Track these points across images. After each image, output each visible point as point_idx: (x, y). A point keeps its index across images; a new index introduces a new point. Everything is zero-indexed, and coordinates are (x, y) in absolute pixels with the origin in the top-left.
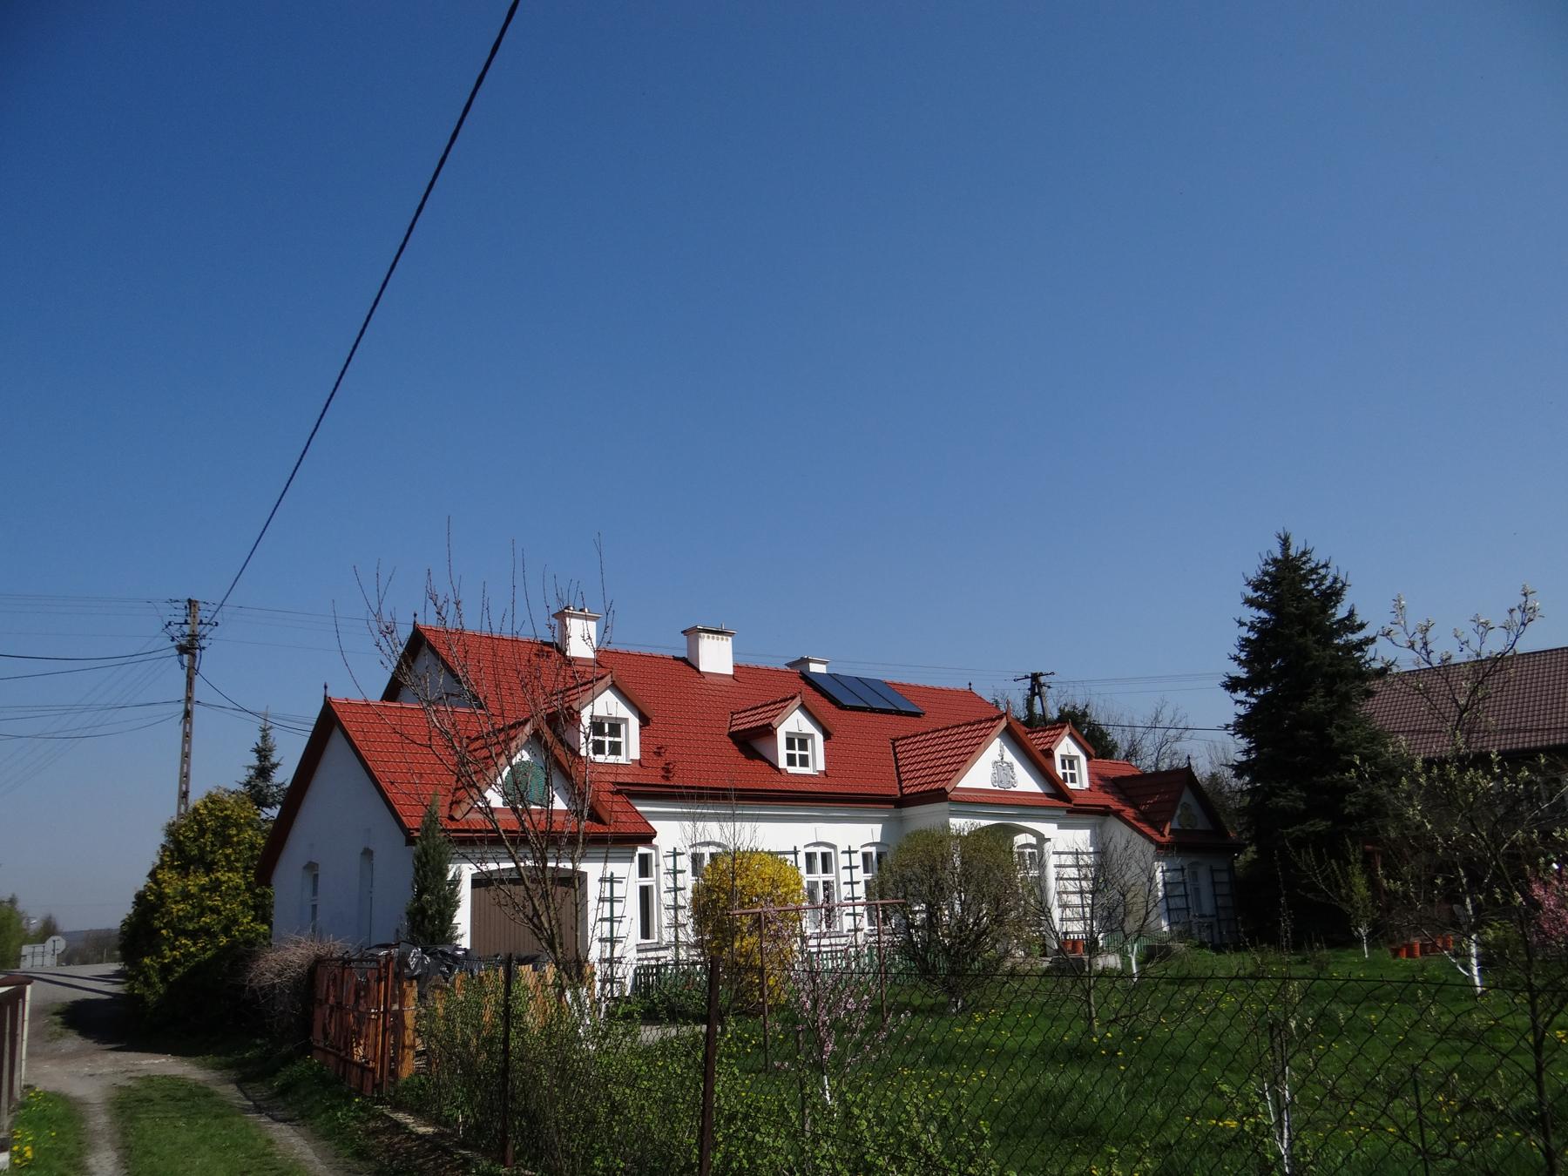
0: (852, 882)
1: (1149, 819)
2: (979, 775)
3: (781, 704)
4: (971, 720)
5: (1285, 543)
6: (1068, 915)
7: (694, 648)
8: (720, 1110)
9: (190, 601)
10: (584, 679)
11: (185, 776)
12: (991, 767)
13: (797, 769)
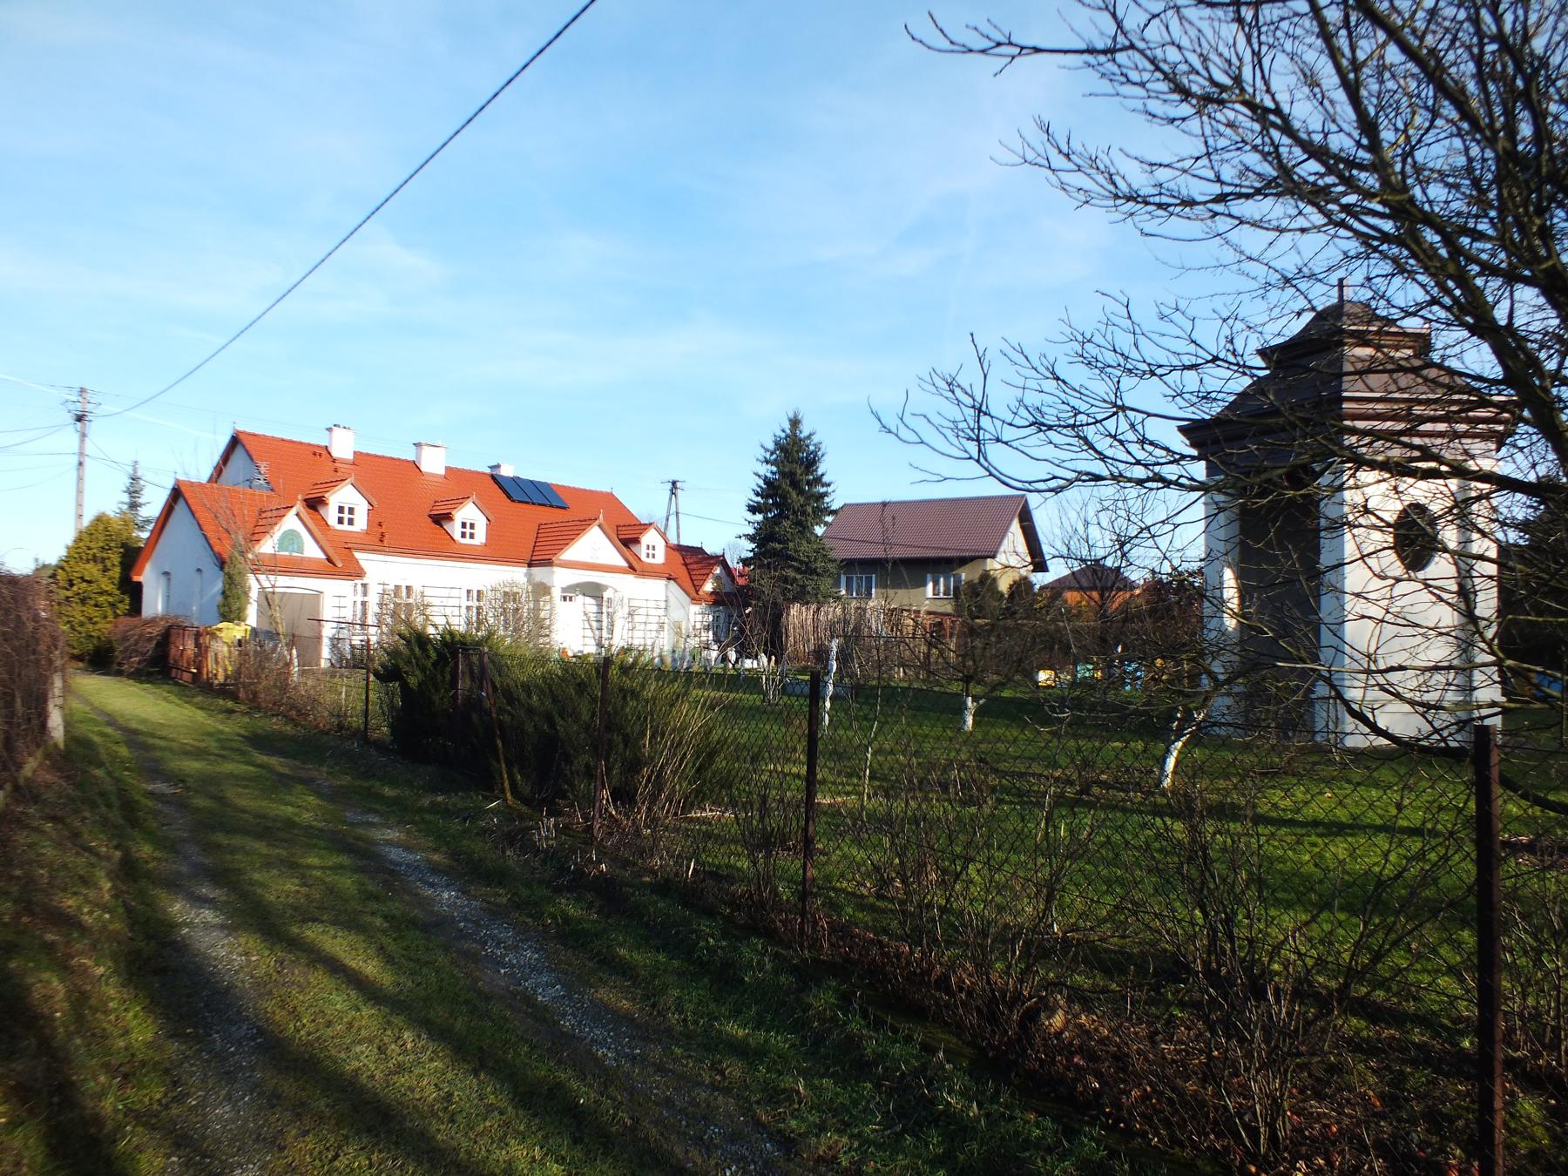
2: (578, 550)
5: (795, 423)
7: (419, 455)
8: (1513, 896)
9: (83, 391)
11: (79, 505)
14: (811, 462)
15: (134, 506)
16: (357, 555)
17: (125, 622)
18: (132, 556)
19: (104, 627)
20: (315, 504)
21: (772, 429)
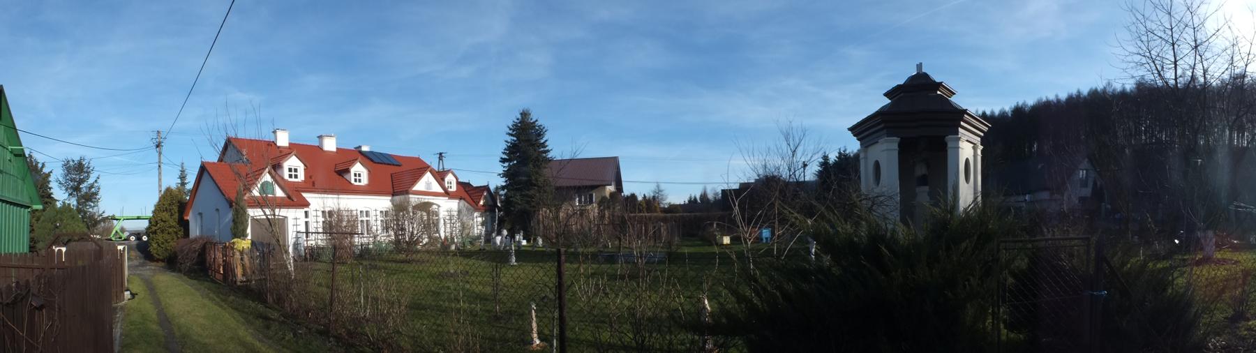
0: (377, 224)
1: (474, 203)
2: (420, 186)
3: (352, 162)
4: (419, 169)
7: (321, 143)
12: (427, 182)
13: (293, 180)
15: (183, 184)
16: (305, 195)
17: (182, 241)
18: (183, 207)
19: (173, 244)
20: (277, 167)
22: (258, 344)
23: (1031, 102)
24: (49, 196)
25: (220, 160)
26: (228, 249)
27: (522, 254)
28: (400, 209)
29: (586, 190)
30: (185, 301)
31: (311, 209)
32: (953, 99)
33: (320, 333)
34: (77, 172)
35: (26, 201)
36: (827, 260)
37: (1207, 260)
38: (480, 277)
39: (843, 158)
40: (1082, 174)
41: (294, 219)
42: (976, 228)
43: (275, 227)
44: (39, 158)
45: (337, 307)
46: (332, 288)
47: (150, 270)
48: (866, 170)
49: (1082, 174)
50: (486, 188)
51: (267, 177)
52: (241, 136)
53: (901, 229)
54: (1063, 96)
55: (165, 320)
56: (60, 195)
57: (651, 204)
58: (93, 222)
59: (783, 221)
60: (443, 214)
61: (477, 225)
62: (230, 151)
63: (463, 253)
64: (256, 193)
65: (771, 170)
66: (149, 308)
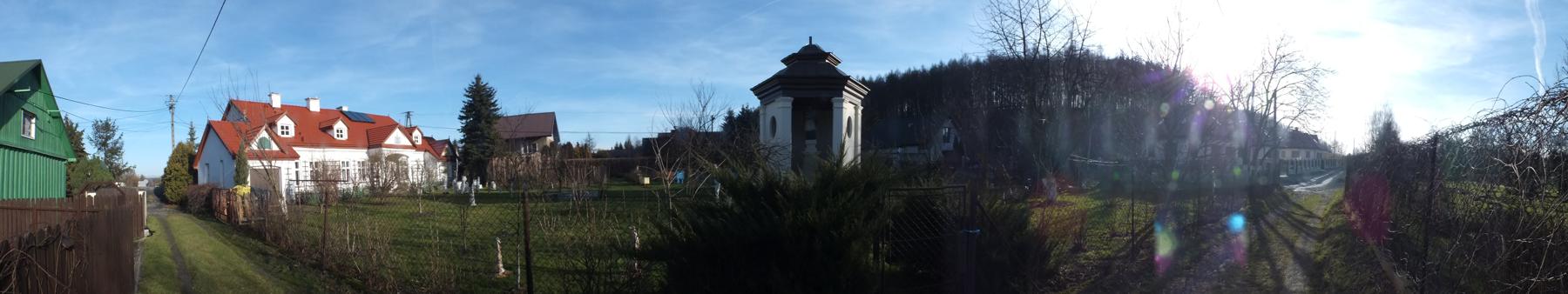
0: (354, 170)
2: (390, 140)
3: (335, 120)
4: (390, 126)
5: (478, 79)
6: (896, 268)
10: (277, 114)
12: (396, 137)
14: (490, 94)
18: (192, 159)
20: (272, 125)
21: (469, 82)
22: (259, 277)
23: (903, 70)
24: (82, 150)
25: (224, 119)
26: (231, 195)
27: (480, 197)
28: (374, 159)
29: (531, 140)
30: (196, 241)
31: (300, 161)
32: (839, 67)
33: (314, 267)
34: (105, 130)
35: (63, 155)
36: (730, 201)
37: (1050, 203)
38: (448, 218)
39: (746, 114)
40: (945, 131)
41: (286, 168)
42: (864, 180)
43: (271, 175)
44: (74, 119)
45: (329, 245)
46: (325, 229)
47: (165, 211)
48: (764, 124)
49: (945, 131)
50: (448, 141)
51: (264, 134)
52: (242, 98)
53: (792, 177)
54: (928, 67)
55: (177, 253)
56: (91, 150)
57: (584, 150)
58: (118, 172)
59: (695, 166)
60: (411, 163)
61: (440, 172)
62: (233, 111)
63: (428, 197)
64: (254, 146)
65: (685, 123)
66: (165, 246)
